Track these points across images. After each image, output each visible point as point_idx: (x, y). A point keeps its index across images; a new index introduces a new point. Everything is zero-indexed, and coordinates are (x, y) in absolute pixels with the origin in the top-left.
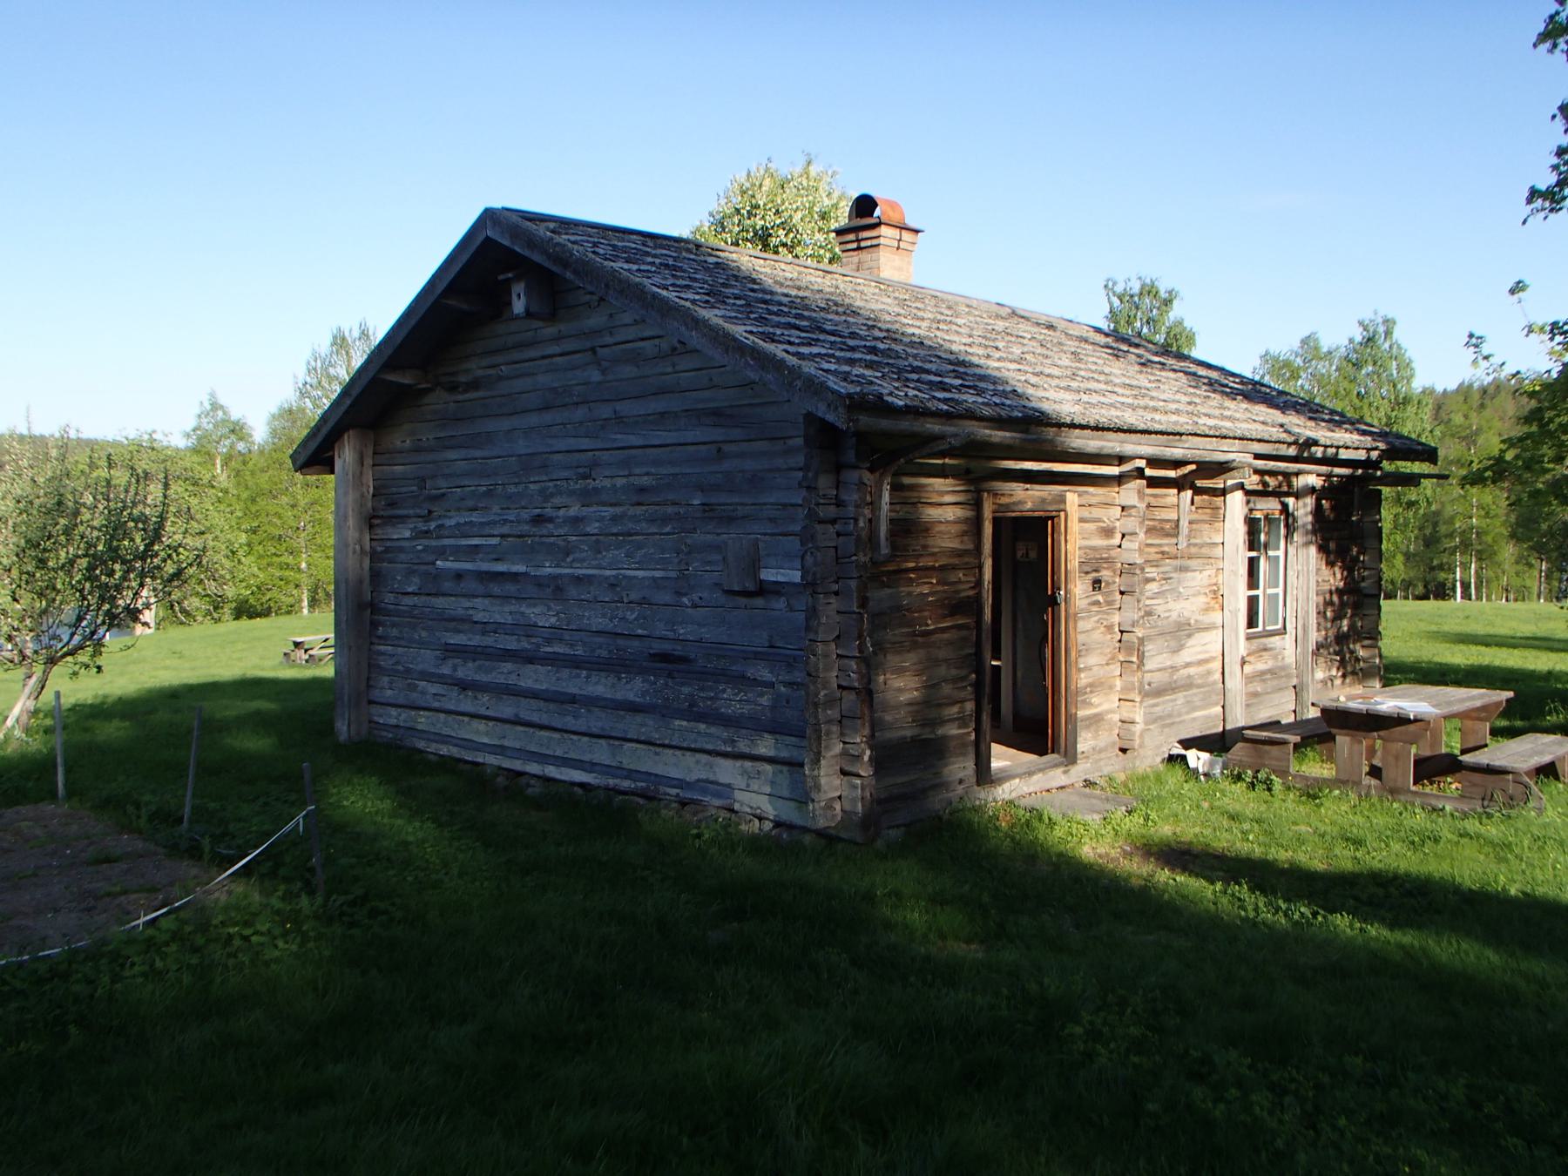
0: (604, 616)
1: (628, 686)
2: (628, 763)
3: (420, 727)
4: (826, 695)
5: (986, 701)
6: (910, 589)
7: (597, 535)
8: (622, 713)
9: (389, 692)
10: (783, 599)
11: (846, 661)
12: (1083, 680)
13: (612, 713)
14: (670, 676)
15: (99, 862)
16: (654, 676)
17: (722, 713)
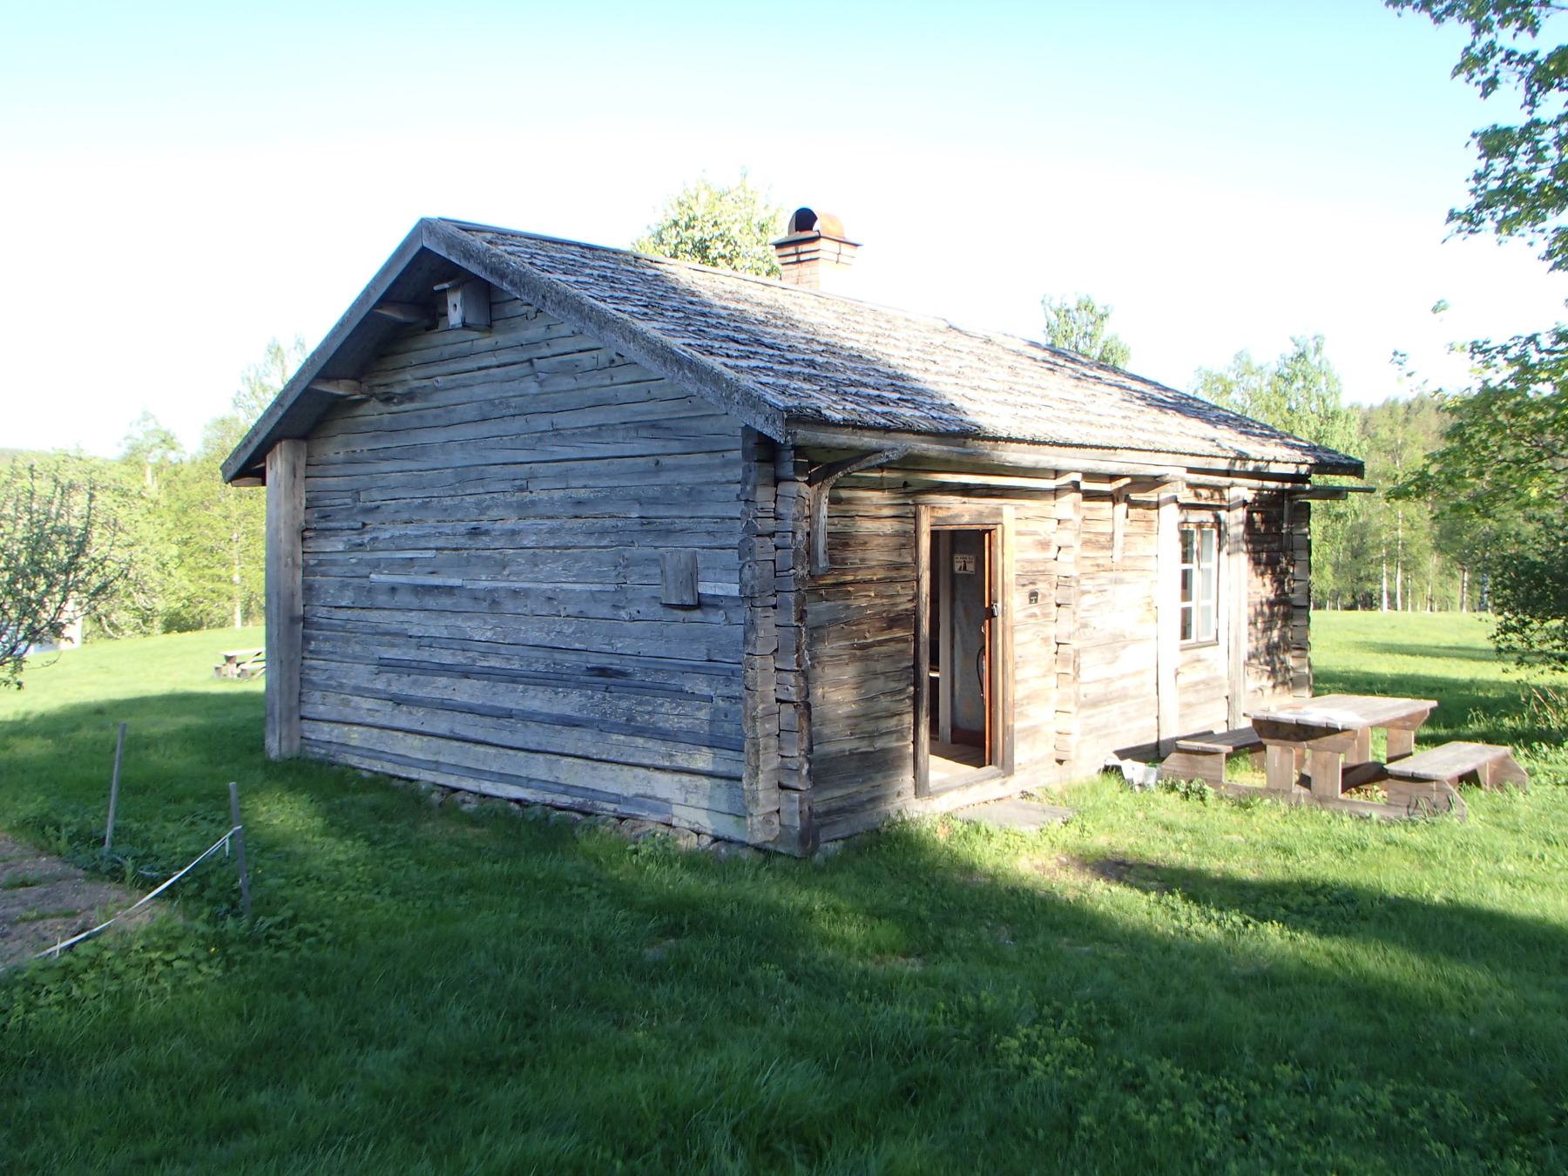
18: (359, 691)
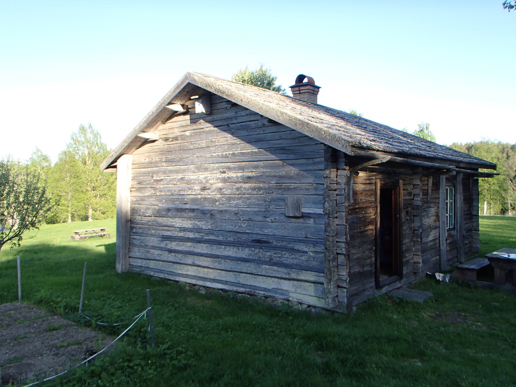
0: (232, 225)
1: (243, 252)
2: (242, 281)
3: (151, 267)
4: (333, 257)
5: (378, 257)
6: (357, 216)
7: (229, 194)
8: (240, 262)
9: (138, 254)
10: (312, 219)
11: (340, 244)
12: (404, 248)
13: (235, 262)
14: (261, 248)
15: (51, 330)
16: (254, 248)
17: (284, 263)
18: (154, 248)
